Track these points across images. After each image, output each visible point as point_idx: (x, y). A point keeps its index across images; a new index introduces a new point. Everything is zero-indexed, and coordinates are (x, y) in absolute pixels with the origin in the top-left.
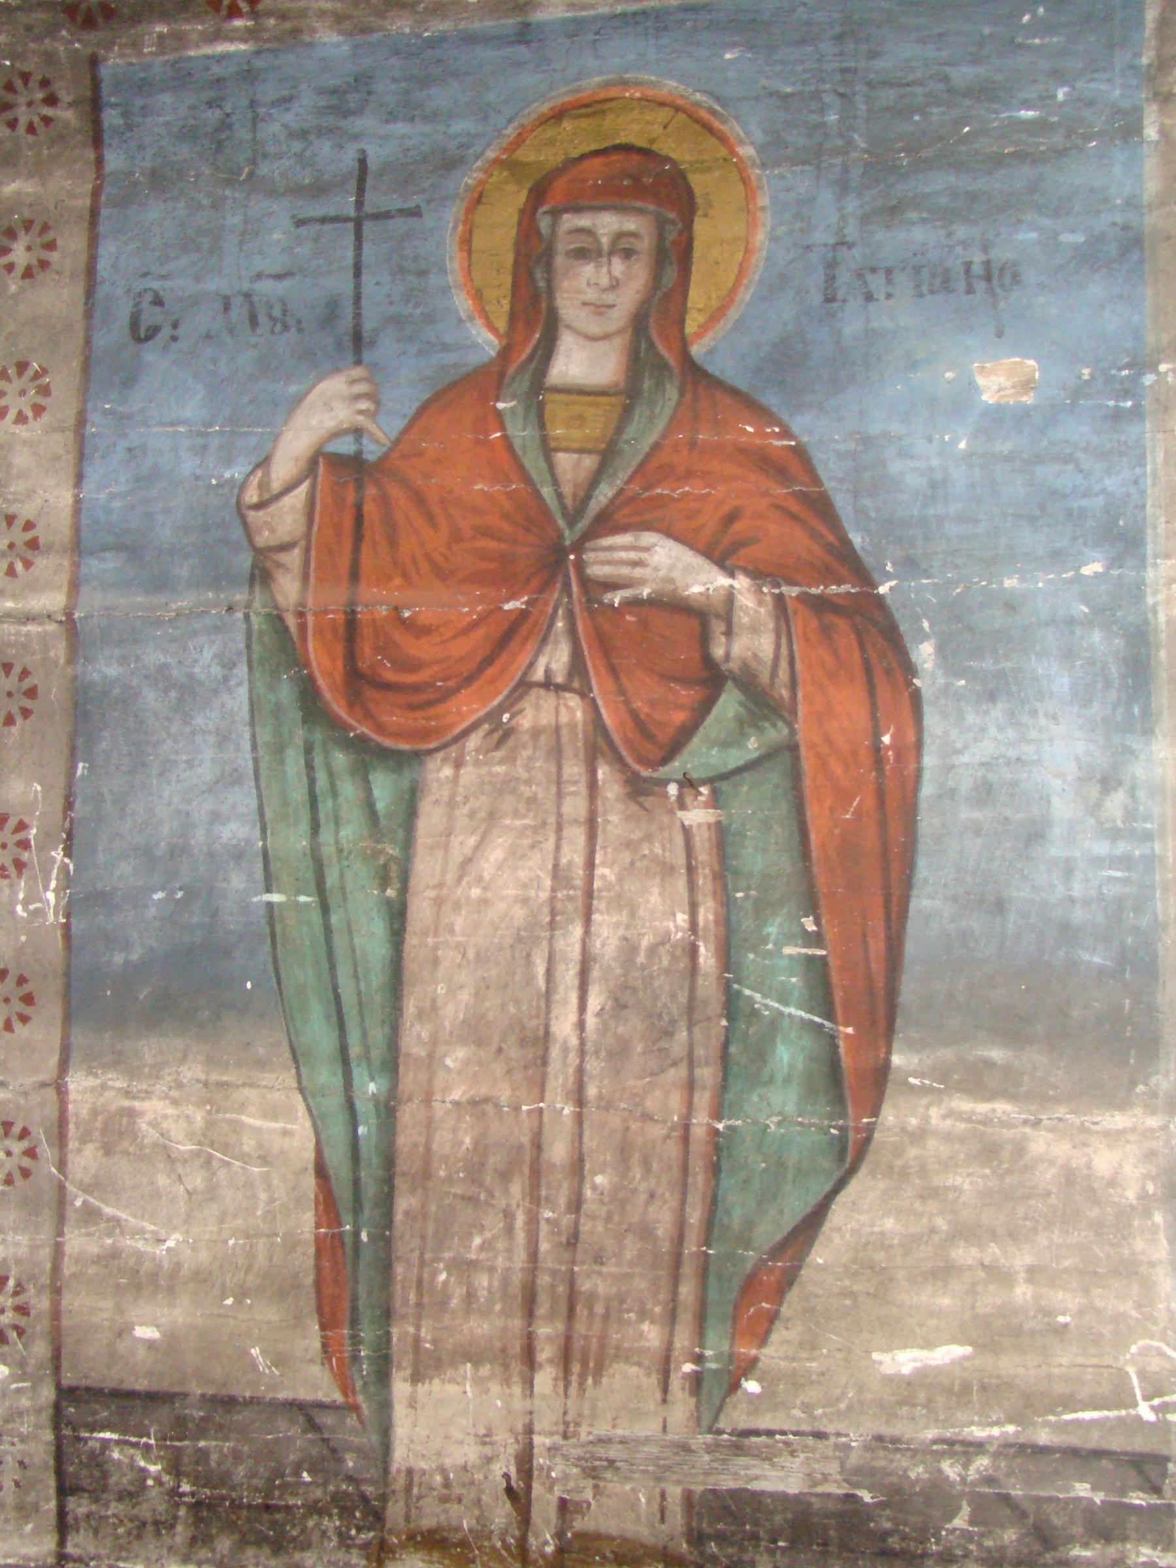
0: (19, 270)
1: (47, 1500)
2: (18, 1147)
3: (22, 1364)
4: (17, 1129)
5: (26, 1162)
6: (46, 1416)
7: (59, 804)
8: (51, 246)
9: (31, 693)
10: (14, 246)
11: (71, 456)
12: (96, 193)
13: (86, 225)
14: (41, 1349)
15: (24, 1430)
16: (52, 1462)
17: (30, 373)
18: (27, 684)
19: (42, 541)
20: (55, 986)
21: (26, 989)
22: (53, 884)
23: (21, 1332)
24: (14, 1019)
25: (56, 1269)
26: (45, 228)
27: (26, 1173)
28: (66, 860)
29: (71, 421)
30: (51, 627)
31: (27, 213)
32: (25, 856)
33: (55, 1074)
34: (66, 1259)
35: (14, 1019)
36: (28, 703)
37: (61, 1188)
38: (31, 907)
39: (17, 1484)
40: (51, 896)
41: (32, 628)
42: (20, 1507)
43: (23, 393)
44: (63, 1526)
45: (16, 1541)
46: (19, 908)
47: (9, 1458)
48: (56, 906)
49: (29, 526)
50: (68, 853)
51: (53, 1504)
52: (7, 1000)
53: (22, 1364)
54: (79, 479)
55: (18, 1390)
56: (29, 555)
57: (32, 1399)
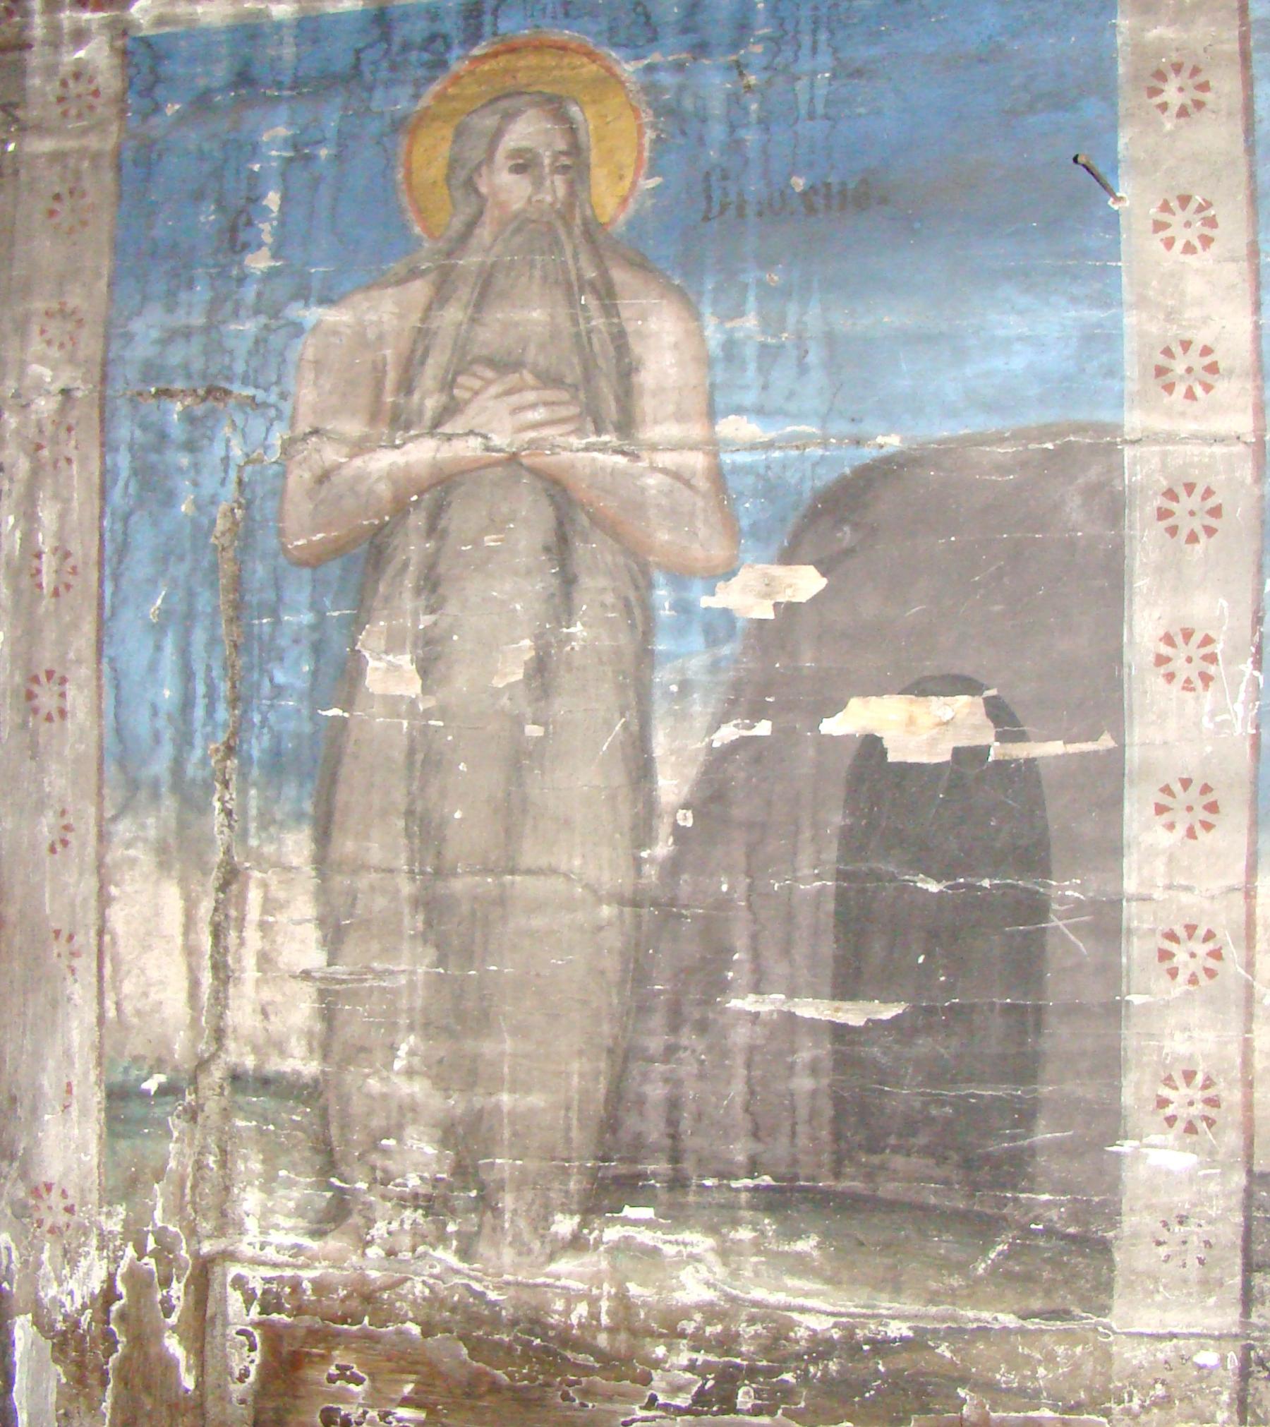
0: (1174, 109)
1: (1233, 1276)
2: (1202, 949)
3: (1212, 1153)
4: (1201, 932)
5: (1211, 963)
6: (1237, 1200)
7: (1247, 621)
8: (1204, 87)
9: (1216, 512)
10: (1166, 88)
11: (1247, 285)
12: (1244, 38)
13: (1238, 67)
14: (1232, 1139)
15: (1213, 1213)
16: (1239, 1242)
17: (1193, 206)
18: (1211, 502)
19: (1222, 366)
20: (1242, 794)
21: (1210, 798)
22: (1242, 696)
23: (1210, 1123)
24: (1198, 827)
25: (1247, 1063)
26: (1195, 71)
27: (1211, 973)
28: (1256, 673)
29: (1243, 251)
30: (1239, 448)
31: (1174, 57)
32: (1212, 670)
33: (1243, 878)
34: (1256, 1054)
35: (1198, 827)
36: (1212, 522)
37: (1249, 987)
38: (1218, 719)
39: (1201, 1261)
40: (1239, 707)
41: (1218, 450)
42: (1204, 1282)
43: (1188, 224)
44: (1248, 1299)
45: (1198, 1312)
46: (1205, 720)
47: (1195, 1238)
48: (1244, 719)
49: (1206, 351)
50: (1258, 664)
51: (1238, 1279)
52: (1190, 809)
53: (1212, 1153)
54: (1257, 306)
55: (1206, 1176)
56: (1209, 378)
57: (1222, 1184)
